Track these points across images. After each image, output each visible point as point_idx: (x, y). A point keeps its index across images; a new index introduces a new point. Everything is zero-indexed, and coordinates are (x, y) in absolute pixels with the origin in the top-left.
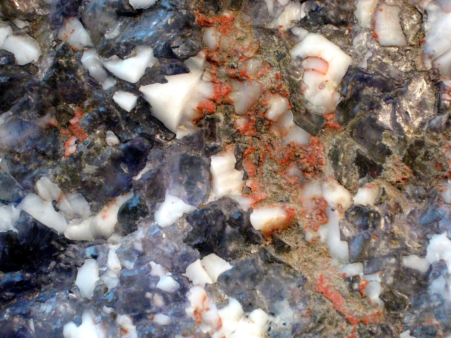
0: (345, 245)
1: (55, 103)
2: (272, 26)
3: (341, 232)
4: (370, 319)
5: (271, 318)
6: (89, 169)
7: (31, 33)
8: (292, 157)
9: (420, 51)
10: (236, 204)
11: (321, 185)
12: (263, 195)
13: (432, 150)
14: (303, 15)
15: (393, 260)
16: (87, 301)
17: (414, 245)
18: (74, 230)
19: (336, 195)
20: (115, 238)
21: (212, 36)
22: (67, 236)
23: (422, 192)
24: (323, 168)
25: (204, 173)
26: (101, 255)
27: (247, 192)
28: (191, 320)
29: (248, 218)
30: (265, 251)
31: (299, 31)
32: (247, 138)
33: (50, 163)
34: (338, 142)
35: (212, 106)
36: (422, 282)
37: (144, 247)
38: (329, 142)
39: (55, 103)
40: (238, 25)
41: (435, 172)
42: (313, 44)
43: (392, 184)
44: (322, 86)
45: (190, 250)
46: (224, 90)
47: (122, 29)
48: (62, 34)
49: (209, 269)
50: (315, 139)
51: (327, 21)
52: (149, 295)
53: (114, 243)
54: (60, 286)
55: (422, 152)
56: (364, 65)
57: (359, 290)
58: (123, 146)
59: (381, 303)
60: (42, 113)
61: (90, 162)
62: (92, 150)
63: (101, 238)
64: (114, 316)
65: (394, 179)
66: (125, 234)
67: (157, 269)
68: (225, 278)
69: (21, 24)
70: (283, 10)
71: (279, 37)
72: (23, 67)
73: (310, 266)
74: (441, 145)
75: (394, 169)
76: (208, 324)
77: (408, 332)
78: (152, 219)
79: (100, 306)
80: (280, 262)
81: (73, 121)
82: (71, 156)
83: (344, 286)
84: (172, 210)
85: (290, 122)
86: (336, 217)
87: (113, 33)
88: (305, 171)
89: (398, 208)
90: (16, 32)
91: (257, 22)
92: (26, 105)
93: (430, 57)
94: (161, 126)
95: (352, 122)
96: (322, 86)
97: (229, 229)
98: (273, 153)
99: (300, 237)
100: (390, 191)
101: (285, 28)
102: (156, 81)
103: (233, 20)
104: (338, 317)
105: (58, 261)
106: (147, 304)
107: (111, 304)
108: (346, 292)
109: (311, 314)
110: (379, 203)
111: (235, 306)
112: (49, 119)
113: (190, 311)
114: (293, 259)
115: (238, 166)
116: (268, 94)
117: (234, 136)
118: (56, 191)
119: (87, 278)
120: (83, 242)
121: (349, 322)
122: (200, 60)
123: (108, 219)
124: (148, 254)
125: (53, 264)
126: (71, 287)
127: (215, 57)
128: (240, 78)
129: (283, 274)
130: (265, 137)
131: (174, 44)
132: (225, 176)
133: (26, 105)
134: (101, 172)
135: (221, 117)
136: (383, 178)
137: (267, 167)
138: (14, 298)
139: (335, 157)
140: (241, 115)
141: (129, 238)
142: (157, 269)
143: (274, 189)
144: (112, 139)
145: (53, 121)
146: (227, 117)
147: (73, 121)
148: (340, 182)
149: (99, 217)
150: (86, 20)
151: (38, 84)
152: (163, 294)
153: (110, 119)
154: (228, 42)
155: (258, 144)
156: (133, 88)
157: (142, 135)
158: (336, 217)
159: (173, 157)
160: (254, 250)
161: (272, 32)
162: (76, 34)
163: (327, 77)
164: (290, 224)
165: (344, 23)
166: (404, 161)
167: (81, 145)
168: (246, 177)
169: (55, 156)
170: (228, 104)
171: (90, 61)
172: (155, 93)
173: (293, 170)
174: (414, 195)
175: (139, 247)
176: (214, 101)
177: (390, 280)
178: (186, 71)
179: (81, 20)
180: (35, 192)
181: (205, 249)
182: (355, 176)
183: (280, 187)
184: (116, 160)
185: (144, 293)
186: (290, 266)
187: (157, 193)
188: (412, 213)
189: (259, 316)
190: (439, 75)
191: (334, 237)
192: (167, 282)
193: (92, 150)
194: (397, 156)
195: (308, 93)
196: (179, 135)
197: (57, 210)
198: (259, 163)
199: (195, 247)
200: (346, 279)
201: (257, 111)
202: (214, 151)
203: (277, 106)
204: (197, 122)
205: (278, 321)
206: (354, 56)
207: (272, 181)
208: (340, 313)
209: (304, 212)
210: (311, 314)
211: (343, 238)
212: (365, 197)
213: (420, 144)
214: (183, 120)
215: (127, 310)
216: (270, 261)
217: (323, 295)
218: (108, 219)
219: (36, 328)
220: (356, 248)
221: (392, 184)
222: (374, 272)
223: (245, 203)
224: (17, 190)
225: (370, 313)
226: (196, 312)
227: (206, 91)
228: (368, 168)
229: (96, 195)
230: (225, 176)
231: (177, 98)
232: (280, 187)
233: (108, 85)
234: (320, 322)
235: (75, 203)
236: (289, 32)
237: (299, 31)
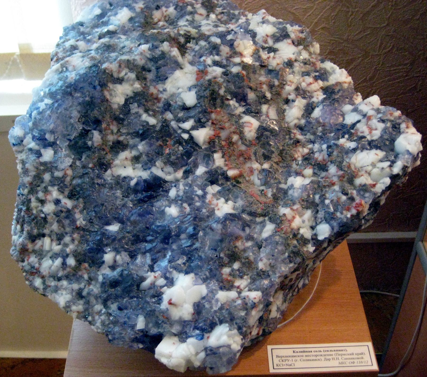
0: (259, 181)
1: (162, 137)
2: (233, 113)
3: (258, 177)
4: (268, 202)
5: (235, 204)
6: (173, 157)
7: (154, 116)
8: (241, 154)
9: (283, 121)
10: (222, 169)
11: (251, 163)
12: (232, 166)
13: (288, 151)
14: (244, 110)
15: (276, 185)
16: (173, 200)
17: (283, 181)
18: (168, 178)
19: (256, 166)
20: (182, 180)
21: (213, 116)
22: (166, 179)
23: (285, 165)
24: (251, 158)
25: (211, 158)
26: (177, 186)
27: (226, 165)
28: (208, 204)
29: (227, 172)
30: (232, 183)
31: (242, 115)
32: (226, 148)
33: (160, 157)
34: (256, 149)
35: (214, 137)
36: (285, 192)
37: (192, 182)
38: (253, 149)
39: (162, 137)
40: (222, 113)
41: (290, 159)
42: (247, 118)
43: (275, 162)
44: (250, 131)
45: (207, 182)
46: (218, 132)
47: (184, 114)
48: (164, 116)
49: (213, 189)
50: (249, 148)
51: (252, 112)
52: (193, 196)
53: (181, 182)
54: (163, 196)
55: (285, 152)
56: (264, 125)
57: (264, 194)
58: (185, 151)
59: (272, 197)
60: (158, 141)
61: (174, 155)
62: (174, 152)
63: (177, 181)
64: (182, 204)
65: (275, 161)
66: (185, 179)
67: (196, 189)
68: (219, 192)
69: (151, 113)
70: (237, 109)
71: (236, 117)
72: (151, 126)
73: (248, 188)
74: (291, 150)
75: (275, 158)
76: (213, 205)
77: (281, 206)
78: (194, 174)
79: (177, 201)
80: (237, 186)
81: (168, 143)
82: (167, 154)
83: (259, 193)
84: (201, 170)
85: (240, 143)
86: (256, 172)
87: (181, 115)
88: (245, 159)
89: (277, 170)
90: (149, 115)
91: (228, 112)
92: (153, 137)
93: (287, 123)
94: (197, 145)
95: (261, 142)
96: (250, 131)
97: (220, 177)
98: (235, 153)
99: (244, 179)
100: (274, 165)
101: (238, 114)
102: (195, 130)
103: (220, 111)
104: (257, 202)
105: (163, 188)
106: (193, 199)
107: (181, 200)
108: (260, 194)
109: (248, 201)
110: (271, 168)
111: (222, 200)
112: (160, 143)
113: (207, 201)
114: (242, 186)
115: (223, 157)
116: (232, 134)
117: (222, 148)
118: (162, 165)
119: (173, 193)
120: (171, 182)
121: (261, 204)
122: (210, 123)
123: (180, 174)
124: (193, 184)
125: (161, 189)
126: (167, 196)
127: (215, 122)
128: (222, 128)
129: (239, 190)
130: (232, 148)
131: (201, 118)
132: (218, 160)
133: (153, 137)
134: (177, 158)
135: (217, 141)
136: (272, 161)
137: (233, 158)
138: (148, 201)
139: (255, 154)
140: (224, 141)
141: (187, 180)
142: (196, 189)
143: (235, 164)
144: (181, 148)
145: (161, 143)
146: (219, 142)
147: (168, 143)
148: (257, 161)
149: (177, 173)
150: (172, 111)
151: (156, 131)
152: (198, 196)
153: (180, 142)
154: (219, 117)
155: (229, 150)
156: (187, 132)
157: (190, 147)
158: (256, 172)
159: (202, 154)
160: (229, 183)
161: (233, 115)
162: (169, 116)
163: (252, 128)
164: (241, 175)
165: (257, 113)
166: (279, 155)
167: (171, 150)
168: (225, 161)
169: (162, 154)
170: (219, 137)
171: (173, 124)
172: (195, 133)
173: (241, 159)
174: (283, 166)
175: (190, 182)
176: (215, 136)
177: (275, 191)
178: (205, 127)
179: (170, 111)
180: (155, 166)
181: (212, 183)
182: (262, 160)
183: (237, 164)
184: (182, 155)
185: (192, 196)
186: (241, 188)
187: (196, 166)
188: (282, 172)
189: (230, 203)
190: (290, 129)
191: (256, 179)
192: (200, 192)
193: (174, 152)
194: (276, 153)
195: (246, 134)
196: (203, 148)
197: (163, 171)
198: (230, 157)
199: (209, 181)
200: (260, 190)
201: (229, 139)
202: (215, 152)
203: (235, 138)
204: (209, 143)
205: (237, 205)
206: (262, 123)
207: (234, 162)
208: (258, 201)
209: (245, 172)
210: (248, 201)
211: (259, 179)
212: (266, 166)
213: (283, 150)
214: (204, 143)
215: (186, 202)
216: (234, 186)
217: (252, 196)
218: (180, 174)
219: (156, 210)
220: (263, 180)
221: (275, 162)
222: (269, 188)
223: (225, 168)
224: (149, 165)
225: (268, 200)
226: (209, 201)
227: (212, 133)
228: (267, 158)
229: (175, 165)
230: (218, 160)
231: (202, 135)
232: (237, 164)
233: (179, 131)
234: (251, 204)
235: (169, 169)
236: (239, 115)
237: (242, 115)
